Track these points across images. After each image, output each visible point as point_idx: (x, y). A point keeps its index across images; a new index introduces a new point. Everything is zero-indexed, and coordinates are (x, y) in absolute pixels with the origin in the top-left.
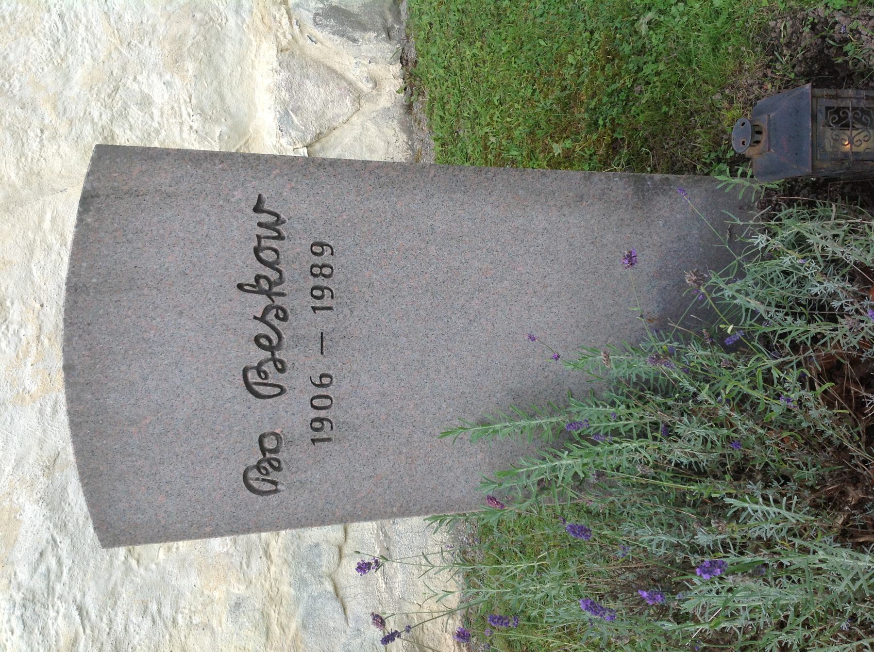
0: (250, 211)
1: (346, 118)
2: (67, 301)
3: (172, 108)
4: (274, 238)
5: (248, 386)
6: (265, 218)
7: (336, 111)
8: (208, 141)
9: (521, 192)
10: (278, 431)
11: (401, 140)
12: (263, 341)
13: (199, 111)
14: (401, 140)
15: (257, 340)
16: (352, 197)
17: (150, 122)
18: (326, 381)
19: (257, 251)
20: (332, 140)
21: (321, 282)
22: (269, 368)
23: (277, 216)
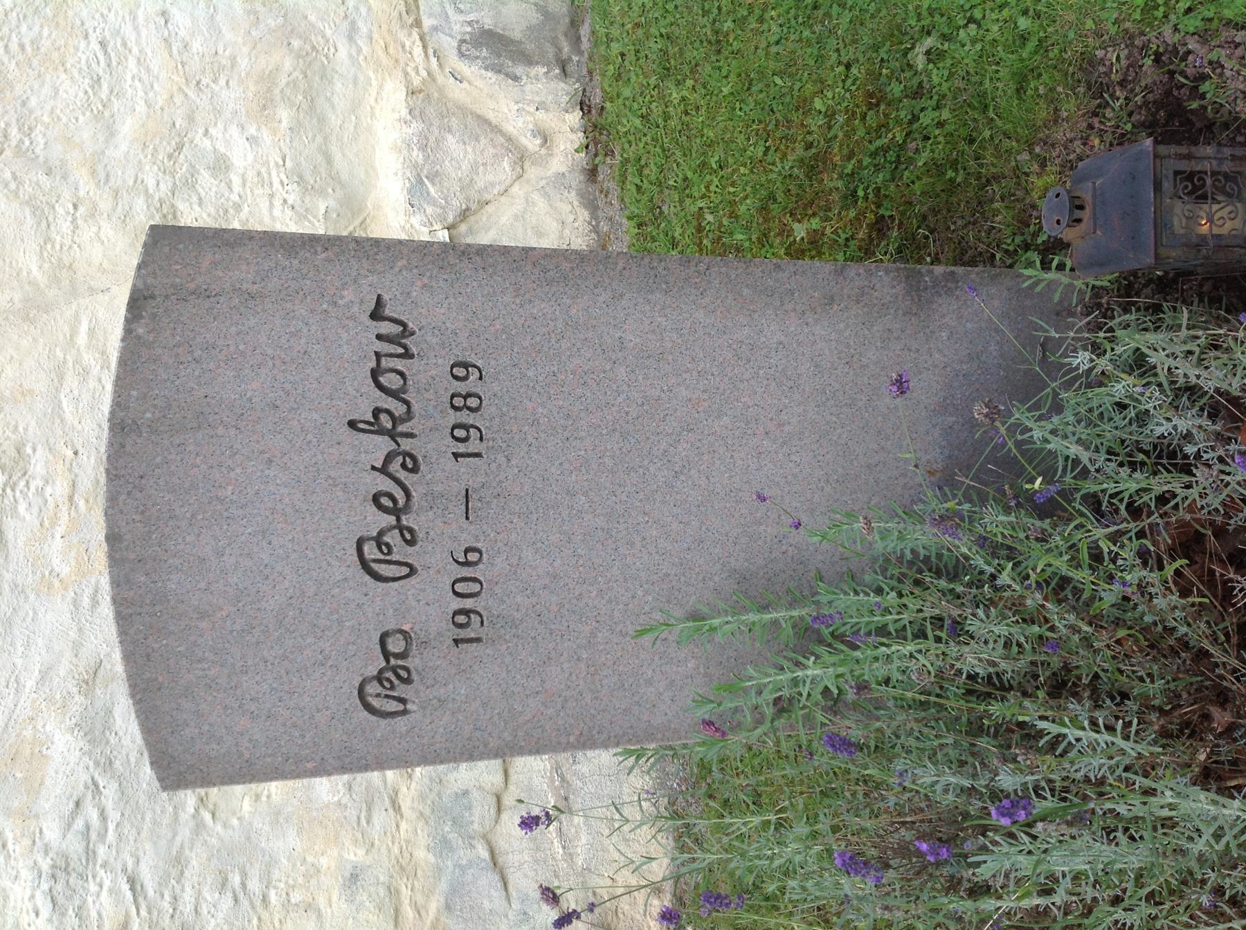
2: (111, 444)
3: (259, 174)
6: (387, 328)
7: (490, 178)
8: (309, 221)
9: (746, 291)
10: (406, 628)
11: (581, 218)
12: (385, 501)
14: (581, 218)
16: (508, 298)
17: (227, 194)
18: (473, 557)
19: (375, 374)
21: (465, 417)
22: (393, 538)
23: (404, 325)
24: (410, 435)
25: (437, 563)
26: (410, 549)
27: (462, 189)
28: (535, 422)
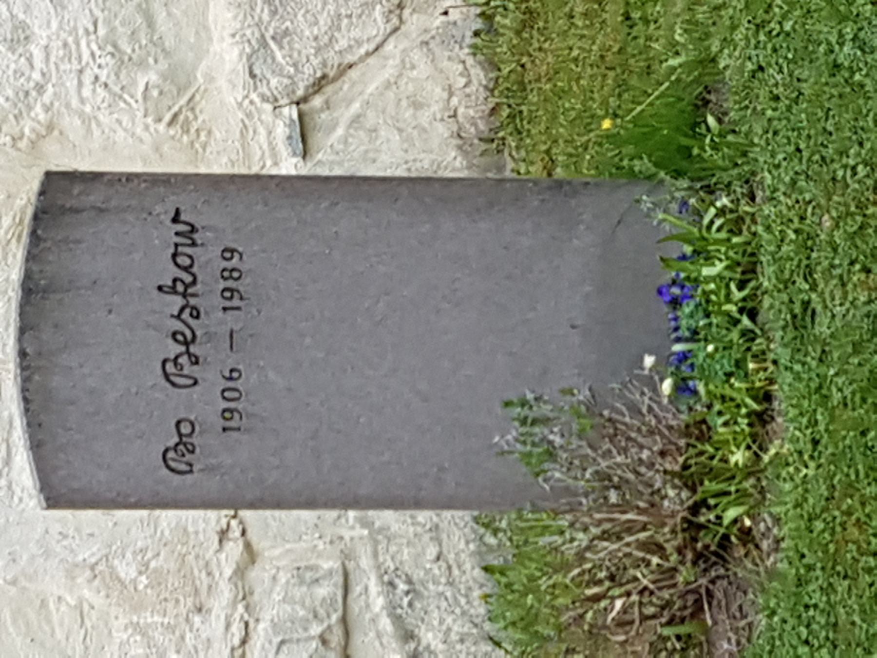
0: (168, 222)
1: (371, 47)
2: (22, 298)
3: (65, 45)
4: (189, 245)
5: (167, 376)
6: (181, 228)
7: (355, 33)
8: (125, 102)
9: (427, 200)
10: (192, 418)
11: (475, 82)
12: (180, 337)
13: (110, 48)
14: (475, 82)
15: (174, 335)
16: (259, 207)
17: (27, 74)
18: (235, 375)
19: (174, 256)
20: (346, 87)
21: (230, 284)
22: (183, 360)
23: (192, 226)
24: (194, 295)
25: (211, 377)
26: (195, 367)
27: (318, 50)
28: (277, 288)
